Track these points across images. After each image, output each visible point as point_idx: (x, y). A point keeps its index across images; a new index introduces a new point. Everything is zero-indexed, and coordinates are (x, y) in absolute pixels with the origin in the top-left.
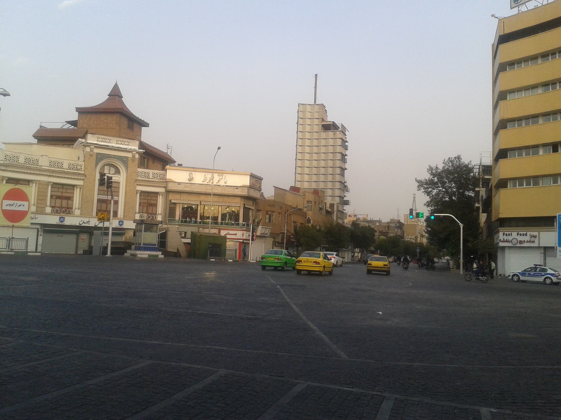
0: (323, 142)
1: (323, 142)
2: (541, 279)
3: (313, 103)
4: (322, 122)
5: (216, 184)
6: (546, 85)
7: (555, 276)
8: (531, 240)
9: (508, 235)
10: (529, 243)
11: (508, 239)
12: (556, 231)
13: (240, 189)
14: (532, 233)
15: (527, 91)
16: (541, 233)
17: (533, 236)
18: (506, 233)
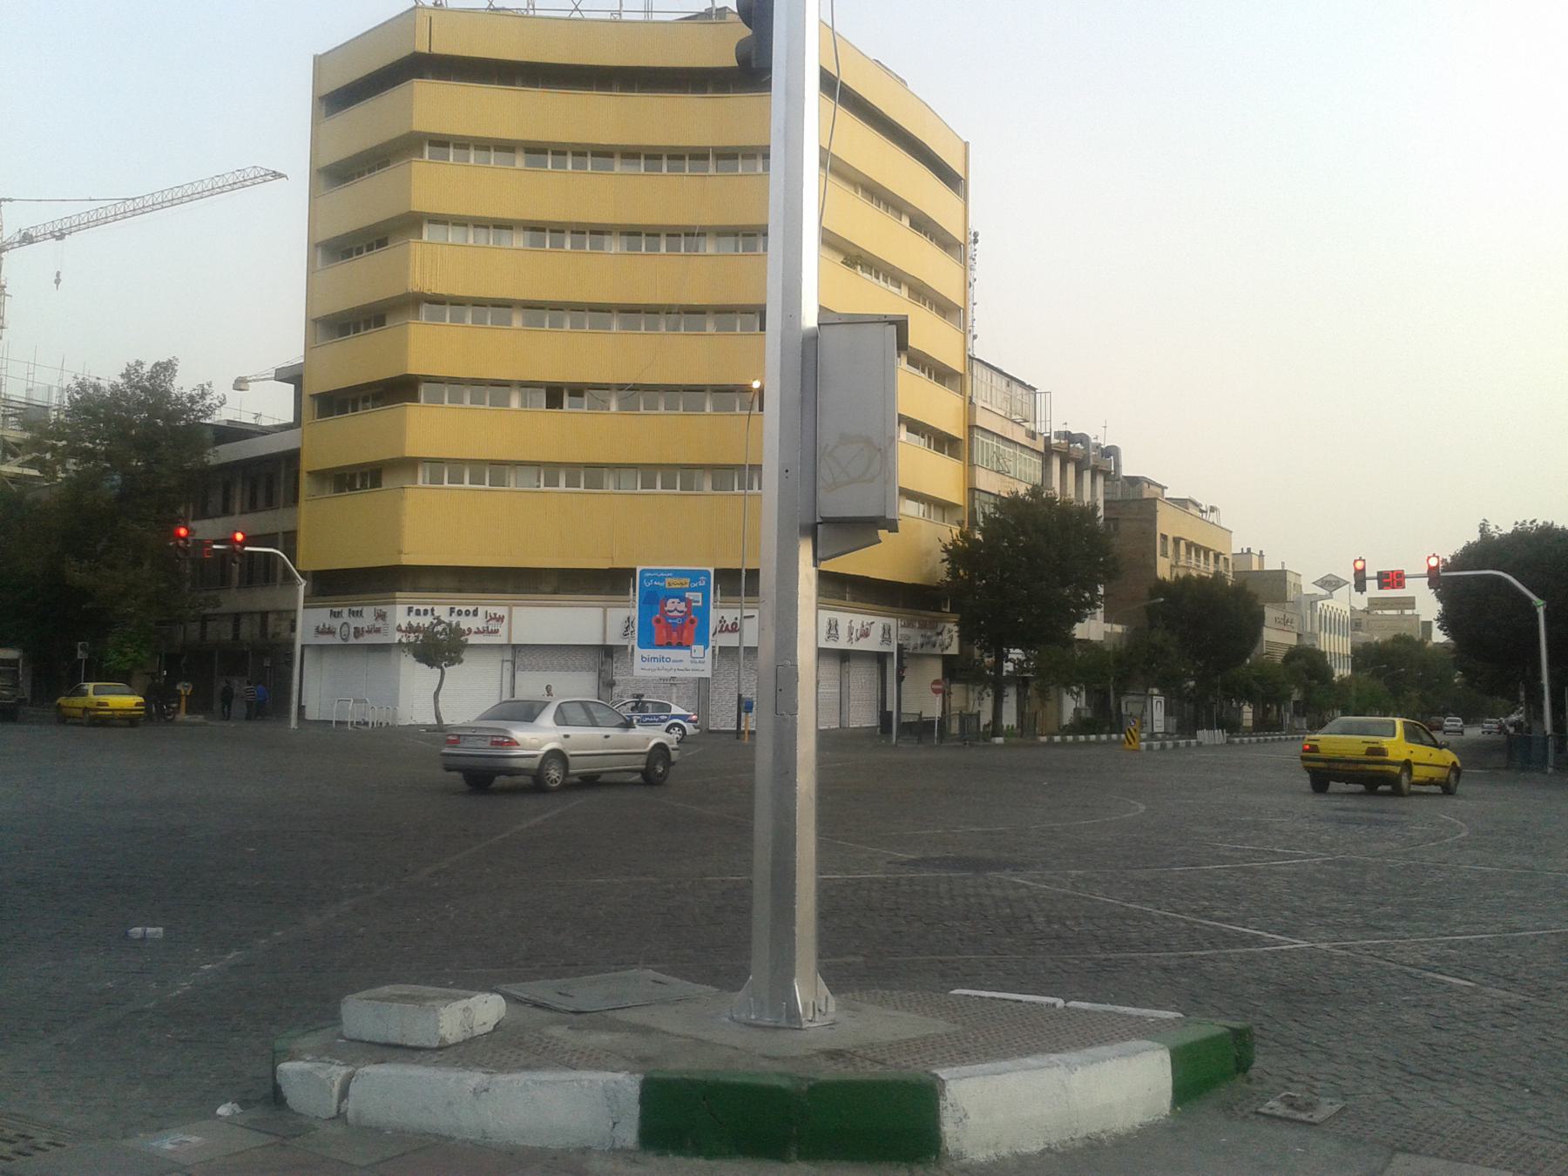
6: (536, 228)
7: (690, 721)
8: (488, 627)
9: (422, 613)
11: (421, 625)
12: (634, 607)
14: (492, 610)
15: (483, 232)
17: (493, 616)
18: (415, 607)
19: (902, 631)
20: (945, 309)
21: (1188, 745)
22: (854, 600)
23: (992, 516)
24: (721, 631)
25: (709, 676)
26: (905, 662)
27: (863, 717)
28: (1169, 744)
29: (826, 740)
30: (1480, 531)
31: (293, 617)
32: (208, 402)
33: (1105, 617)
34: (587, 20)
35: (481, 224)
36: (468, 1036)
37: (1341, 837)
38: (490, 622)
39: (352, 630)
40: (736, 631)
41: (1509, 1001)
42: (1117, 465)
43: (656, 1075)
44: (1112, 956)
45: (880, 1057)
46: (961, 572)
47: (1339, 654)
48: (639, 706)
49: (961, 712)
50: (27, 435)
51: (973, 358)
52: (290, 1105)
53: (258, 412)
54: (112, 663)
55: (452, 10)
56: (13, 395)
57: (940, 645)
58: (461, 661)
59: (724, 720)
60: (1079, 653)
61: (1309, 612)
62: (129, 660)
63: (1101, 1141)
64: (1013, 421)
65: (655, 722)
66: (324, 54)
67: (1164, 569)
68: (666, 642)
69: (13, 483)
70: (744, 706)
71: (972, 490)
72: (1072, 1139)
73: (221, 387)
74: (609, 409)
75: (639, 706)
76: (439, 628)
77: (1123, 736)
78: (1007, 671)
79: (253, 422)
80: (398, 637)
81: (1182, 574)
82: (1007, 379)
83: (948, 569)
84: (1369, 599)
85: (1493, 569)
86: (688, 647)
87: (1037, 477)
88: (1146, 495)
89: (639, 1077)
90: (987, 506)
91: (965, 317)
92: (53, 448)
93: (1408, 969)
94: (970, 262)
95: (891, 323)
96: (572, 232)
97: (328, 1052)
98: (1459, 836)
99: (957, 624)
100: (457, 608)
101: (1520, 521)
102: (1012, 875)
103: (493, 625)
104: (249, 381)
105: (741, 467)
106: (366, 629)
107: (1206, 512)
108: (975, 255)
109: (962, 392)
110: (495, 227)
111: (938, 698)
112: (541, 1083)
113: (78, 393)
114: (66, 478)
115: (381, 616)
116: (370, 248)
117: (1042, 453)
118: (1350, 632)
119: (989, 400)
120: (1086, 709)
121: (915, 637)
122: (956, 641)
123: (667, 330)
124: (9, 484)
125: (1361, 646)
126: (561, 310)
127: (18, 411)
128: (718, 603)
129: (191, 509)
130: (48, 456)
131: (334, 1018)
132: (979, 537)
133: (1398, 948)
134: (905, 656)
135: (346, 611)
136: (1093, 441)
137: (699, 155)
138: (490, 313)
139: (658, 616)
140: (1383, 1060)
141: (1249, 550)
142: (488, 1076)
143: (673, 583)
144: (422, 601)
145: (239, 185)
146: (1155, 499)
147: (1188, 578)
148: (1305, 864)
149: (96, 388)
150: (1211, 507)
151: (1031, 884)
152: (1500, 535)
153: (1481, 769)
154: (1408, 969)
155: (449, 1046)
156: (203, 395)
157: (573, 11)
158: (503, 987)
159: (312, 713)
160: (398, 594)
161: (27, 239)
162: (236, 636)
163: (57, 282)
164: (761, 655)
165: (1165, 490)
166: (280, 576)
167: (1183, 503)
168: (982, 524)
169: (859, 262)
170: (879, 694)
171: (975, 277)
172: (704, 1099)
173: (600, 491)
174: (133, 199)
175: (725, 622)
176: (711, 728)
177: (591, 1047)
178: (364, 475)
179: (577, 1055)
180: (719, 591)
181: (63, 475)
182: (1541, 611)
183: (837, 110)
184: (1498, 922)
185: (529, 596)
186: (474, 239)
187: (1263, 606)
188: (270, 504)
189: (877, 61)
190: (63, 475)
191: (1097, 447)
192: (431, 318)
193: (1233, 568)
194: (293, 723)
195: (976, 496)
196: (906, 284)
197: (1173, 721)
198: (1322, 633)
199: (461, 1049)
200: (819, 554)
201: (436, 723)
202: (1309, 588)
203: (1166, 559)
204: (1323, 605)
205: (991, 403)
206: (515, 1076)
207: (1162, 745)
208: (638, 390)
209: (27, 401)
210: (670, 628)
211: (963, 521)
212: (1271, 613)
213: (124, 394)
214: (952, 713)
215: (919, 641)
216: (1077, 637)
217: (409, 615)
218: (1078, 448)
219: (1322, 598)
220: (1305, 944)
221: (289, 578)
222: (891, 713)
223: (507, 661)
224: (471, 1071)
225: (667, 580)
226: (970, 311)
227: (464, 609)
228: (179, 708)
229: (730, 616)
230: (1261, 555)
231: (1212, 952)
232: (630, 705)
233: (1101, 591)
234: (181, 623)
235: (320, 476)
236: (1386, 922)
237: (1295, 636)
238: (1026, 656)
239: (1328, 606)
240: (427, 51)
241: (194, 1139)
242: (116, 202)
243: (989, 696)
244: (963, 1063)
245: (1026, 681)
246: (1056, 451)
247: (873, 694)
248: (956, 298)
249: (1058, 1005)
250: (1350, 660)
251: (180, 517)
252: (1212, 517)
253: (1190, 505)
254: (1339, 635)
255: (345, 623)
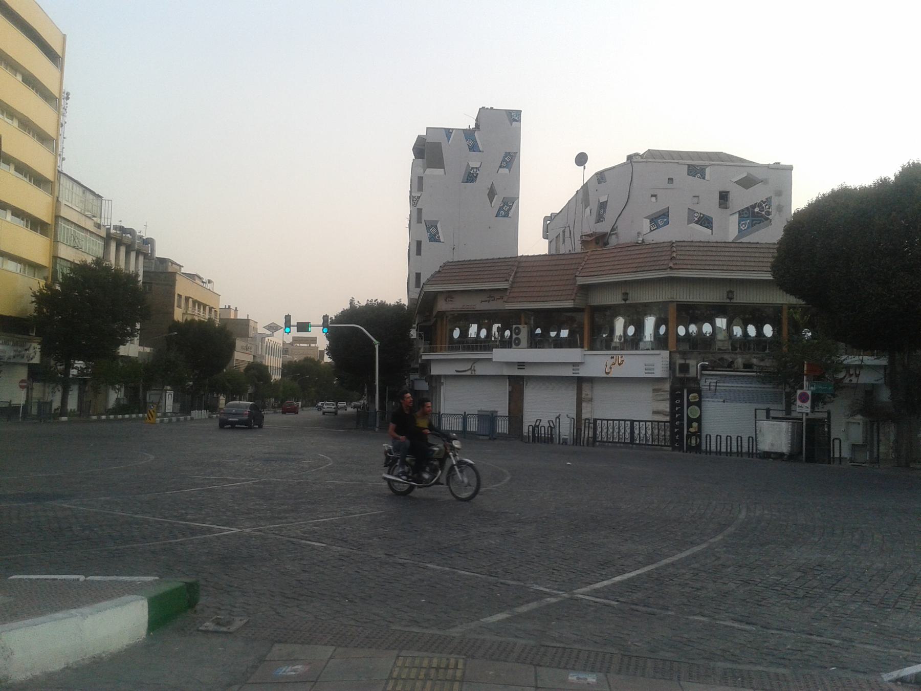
21: (186, 419)
23: (68, 275)
28: (174, 419)
30: (350, 304)
33: (140, 342)
37: (265, 469)
41: (342, 552)
42: (153, 250)
44: (120, 547)
46: (45, 310)
47: (275, 367)
49: (39, 400)
57: (27, 357)
60: (121, 364)
61: (260, 343)
63: (101, 658)
64: (86, 216)
67: (178, 315)
71: (55, 258)
72: (83, 659)
77: (146, 415)
78: (73, 375)
81: (189, 318)
82: (84, 189)
83: (36, 308)
84: (293, 337)
85: (360, 326)
87: (100, 254)
88: (170, 270)
90: (65, 268)
93: (292, 539)
98: (328, 465)
99: (39, 344)
101: (370, 300)
102: (62, 503)
107: (205, 283)
108: (67, 107)
109: (52, 193)
111: (23, 392)
117: (104, 238)
118: (282, 355)
119: (70, 200)
120: (124, 399)
122: (38, 354)
125: (287, 363)
132: (58, 288)
133: (288, 528)
136: (138, 234)
140: (273, 592)
141: (229, 306)
146: (175, 273)
147: (193, 320)
148: (244, 485)
150: (209, 280)
151: (74, 507)
152: (360, 306)
153: (343, 429)
154: (292, 539)
165: (182, 268)
167: (192, 277)
168: (61, 280)
171: (66, 121)
182: (377, 347)
184: (342, 510)
187: (236, 339)
191: (141, 238)
193: (220, 316)
195: (58, 262)
197: (178, 405)
198: (267, 355)
202: (261, 330)
203: (180, 309)
204: (268, 339)
205: (72, 202)
207: (169, 420)
211: (48, 277)
212: (239, 343)
215: (12, 354)
216: (121, 354)
218: (128, 237)
219: (268, 336)
220: (236, 530)
226: (60, 142)
230: (236, 310)
231: (183, 539)
233: (138, 326)
236: (283, 515)
237: (252, 356)
238: (86, 365)
239: (271, 341)
243: (59, 391)
244: (12, 621)
245: (85, 381)
246: (113, 237)
248: (51, 132)
249: (81, 580)
250: (281, 370)
252: (209, 286)
253: (196, 278)
254: (274, 356)
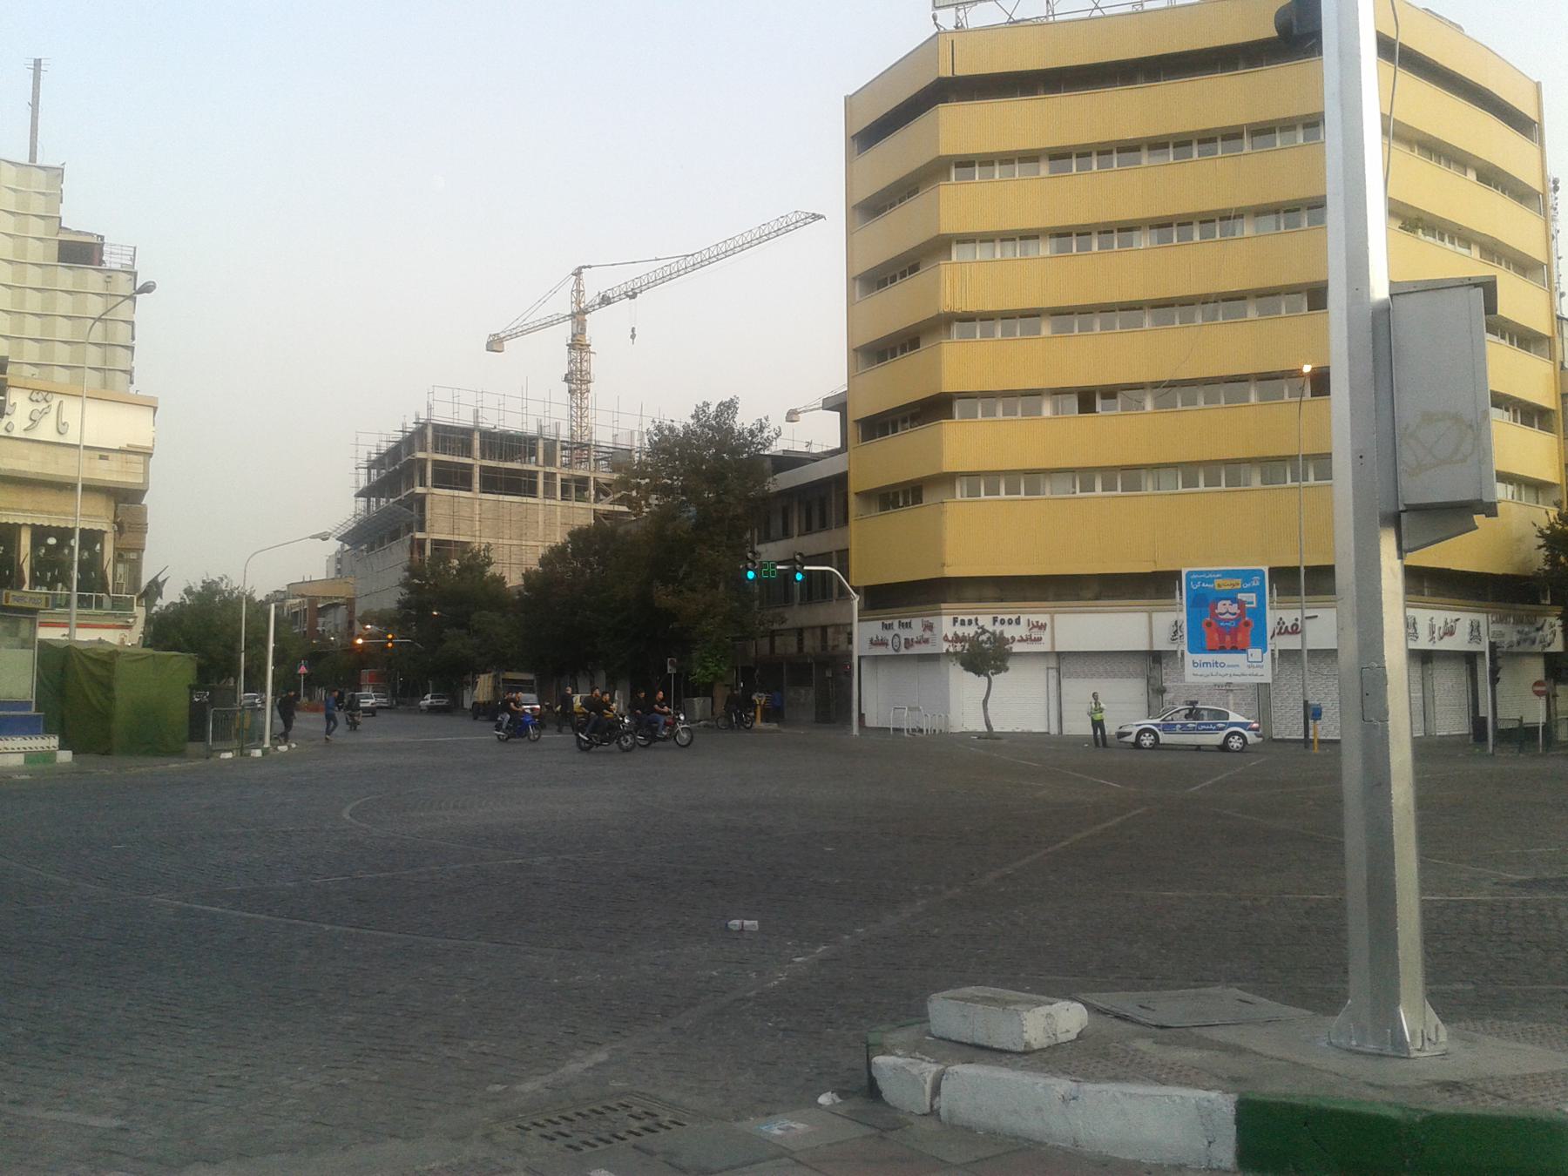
0: (64, 304)
1: (64, 304)
2: (1217, 739)
3: (26, 161)
4: (58, 233)
5: (23, 435)
6: (1061, 234)
7: (1250, 730)
9: (966, 623)
10: (1025, 644)
12: (1181, 611)
13: (115, 463)
14: (1034, 618)
15: (1009, 245)
16: (1057, 617)
17: (1035, 624)
18: (960, 618)
19: (1493, 628)
20: (1525, 266)
22: (1433, 595)
24: (1279, 633)
25: (1270, 681)
26: (1500, 662)
27: (1451, 722)
29: (1426, 749)
31: (849, 630)
32: (765, 435)
34: (1109, 16)
35: (1007, 237)
36: (1053, 1042)
38: (1033, 630)
39: (903, 641)
40: (1299, 632)
43: (1251, 1097)
45: (1502, 1092)
48: (1193, 713)
50: (616, 476)
51: (1563, 319)
52: (885, 1098)
53: (810, 441)
54: (696, 676)
55: (976, 30)
56: (602, 442)
57: (1541, 642)
58: (1007, 669)
59: (1288, 726)
62: (710, 674)
65: (1211, 730)
66: (854, 94)
68: (1230, 646)
69: (605, 518)
70: (1312, 713)
73: (777, 420)
74: (1144, 409)
75: (1193, 713)
76: (984, 637)
79: (804, 450)
80: (945, 646)
86: (1244, 651)
89: (1234, 1097)
91: (1549, 273)
92: (638, 486)
94: (1552, 212)
95: (1476, 285)
96: (1100, 233)
97: (917, 1049)
99: (1560, 617)
100: (1000, 617)
103: (1036, 634)
104: (799, 413)
105: (1292, 459)
106: (915, 640)
108: (1557, 204)
110: (1022, 238)
112: (1131, 1095)
113: (656, 435)
114: (650, 512)
115: (929, 627)
116: (903, 275)
121: (1509, 634)
123: (1203, 321)
124: (603, 519)
126: (1091, 313)
127: (607, 455)
128: (1275, 604)
129: (756, 533)
130: (634, 493)
131: (921, 1016)
134: (1498, 654)
135: (896, 623)
137: (1232, 135)
138: (1018, 325)
139: (1209, 619)
142: (1075, 1084)
143: (1225, 584)
144: (965, 611)
145: (783, 230)
149: (671, 429)
155: (1034, 1051)
156: (761, 430)
157: (1093, 10)
158: (1082, 996)
159: (871, 721)
160: (943, 605)
161: (606, 301)
162: (800, 649)
163: (633, 337)
164: (1342, 657)
166: (835, 591)
169: (1420, 225)
170: (1470, 697)
171: (1558, 228)
172: (1306, 1124)
173: (1139, 493)
174: (693, 255)
175: (1284, 623)
176: (1274, 737)
177: (1179, 1064)
178: (905, 493)
179: (1166, 1070)
180: (1275, 591)
181: (647, 510)
183: (1398, 73)
185: (1071, 603)
186: (1001, 253)
188: (824, 526)
189: (1427, 9)
190: (647, 510)
192: (962, 335)
194: (855, 731)
196: (1476, 243)
199: (1046, 1055)
200: (1405, 546)
201: (986, 730)
206: (1104, 1086)
208: (1175, 386)
209: (614, 446)
210: (1221, 632)
211: (1562, 502)
213: (694, 433)
214: (1559, 717)
215: (1515, 638)
217: (954, 625)
221: (843, 593)
222: (1484, 720)
223: (1052, 668)
224: (1058, 1078)
225: (1217, 582)
226: (1555, 266)
227: (1006, 617)
228: (755, 717)
229: (1290, 616)
232: (1183, 713)
234: (753, 639)
235: (865, 496)
240: (950, 75)
241: (800, 1126)
242: (677, 259)
247: (1464, 699)
248: (1536, 252)
251: (747, 542)
255: (896, 635)
